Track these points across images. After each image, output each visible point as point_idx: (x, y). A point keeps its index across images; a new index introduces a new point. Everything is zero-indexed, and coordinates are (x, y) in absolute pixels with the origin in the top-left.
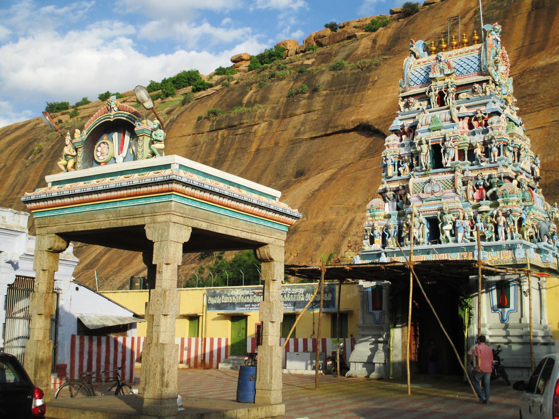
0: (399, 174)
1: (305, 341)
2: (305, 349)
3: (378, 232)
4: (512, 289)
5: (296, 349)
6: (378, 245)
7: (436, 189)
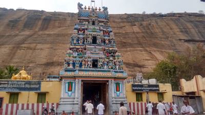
0: (79, 43)
1: (23, 105)
2: (28, 108)
3: (71, 62)
4: (120, 85)
5: (23, 108)
6: (71, 67)
7: (96, 50)
